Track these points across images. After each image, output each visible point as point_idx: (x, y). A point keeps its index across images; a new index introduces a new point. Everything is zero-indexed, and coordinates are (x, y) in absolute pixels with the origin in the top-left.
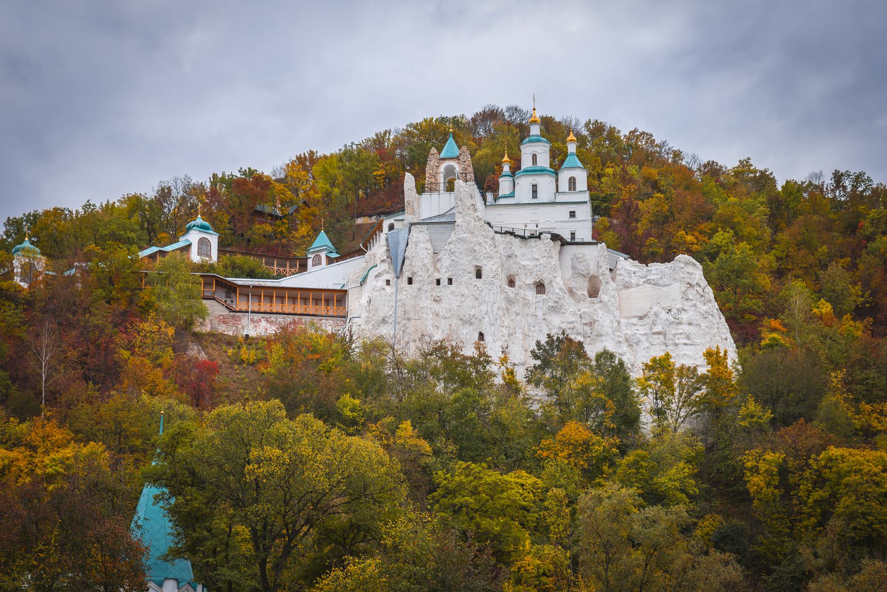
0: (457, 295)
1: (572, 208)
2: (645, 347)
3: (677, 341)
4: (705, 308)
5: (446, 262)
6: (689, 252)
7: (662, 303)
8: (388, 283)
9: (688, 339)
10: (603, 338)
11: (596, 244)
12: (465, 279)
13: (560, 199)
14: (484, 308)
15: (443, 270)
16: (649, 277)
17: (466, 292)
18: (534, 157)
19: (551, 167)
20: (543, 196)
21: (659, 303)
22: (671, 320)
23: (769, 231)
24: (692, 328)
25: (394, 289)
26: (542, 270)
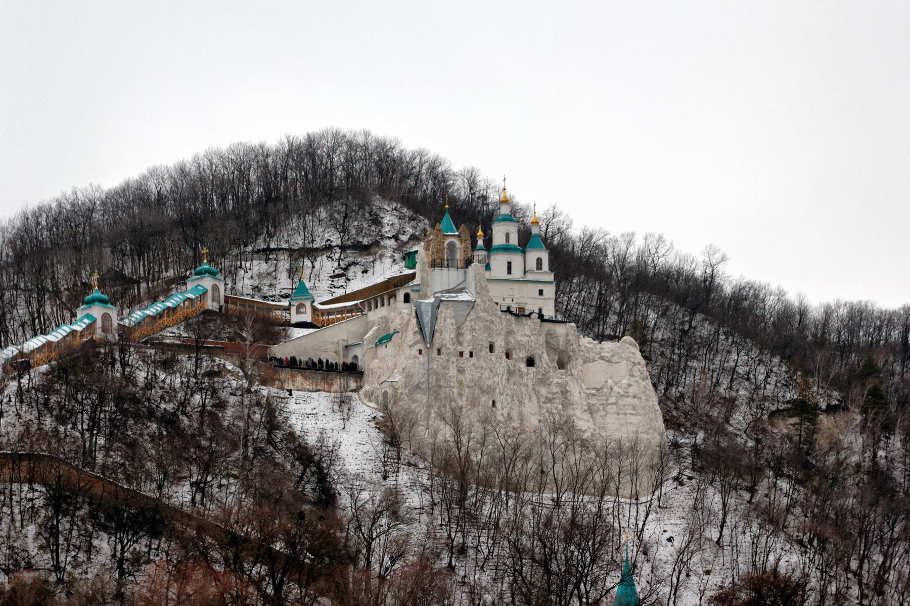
0: (477, 368)
1: (541, 287)
4: (644, 383)
5: (468, 337)
6: (643, 342)
10: (575, 406)
11: (565, 322)
12: (483, 353)
13: (529, 277)
14: (496, 379)
15: (466, 344)
16: (603, 354)
17: (484, 365)
18: (507, 235)
19: (519, 245)
20: (517, 273)
24: (636, 400)
25: (426, 358)
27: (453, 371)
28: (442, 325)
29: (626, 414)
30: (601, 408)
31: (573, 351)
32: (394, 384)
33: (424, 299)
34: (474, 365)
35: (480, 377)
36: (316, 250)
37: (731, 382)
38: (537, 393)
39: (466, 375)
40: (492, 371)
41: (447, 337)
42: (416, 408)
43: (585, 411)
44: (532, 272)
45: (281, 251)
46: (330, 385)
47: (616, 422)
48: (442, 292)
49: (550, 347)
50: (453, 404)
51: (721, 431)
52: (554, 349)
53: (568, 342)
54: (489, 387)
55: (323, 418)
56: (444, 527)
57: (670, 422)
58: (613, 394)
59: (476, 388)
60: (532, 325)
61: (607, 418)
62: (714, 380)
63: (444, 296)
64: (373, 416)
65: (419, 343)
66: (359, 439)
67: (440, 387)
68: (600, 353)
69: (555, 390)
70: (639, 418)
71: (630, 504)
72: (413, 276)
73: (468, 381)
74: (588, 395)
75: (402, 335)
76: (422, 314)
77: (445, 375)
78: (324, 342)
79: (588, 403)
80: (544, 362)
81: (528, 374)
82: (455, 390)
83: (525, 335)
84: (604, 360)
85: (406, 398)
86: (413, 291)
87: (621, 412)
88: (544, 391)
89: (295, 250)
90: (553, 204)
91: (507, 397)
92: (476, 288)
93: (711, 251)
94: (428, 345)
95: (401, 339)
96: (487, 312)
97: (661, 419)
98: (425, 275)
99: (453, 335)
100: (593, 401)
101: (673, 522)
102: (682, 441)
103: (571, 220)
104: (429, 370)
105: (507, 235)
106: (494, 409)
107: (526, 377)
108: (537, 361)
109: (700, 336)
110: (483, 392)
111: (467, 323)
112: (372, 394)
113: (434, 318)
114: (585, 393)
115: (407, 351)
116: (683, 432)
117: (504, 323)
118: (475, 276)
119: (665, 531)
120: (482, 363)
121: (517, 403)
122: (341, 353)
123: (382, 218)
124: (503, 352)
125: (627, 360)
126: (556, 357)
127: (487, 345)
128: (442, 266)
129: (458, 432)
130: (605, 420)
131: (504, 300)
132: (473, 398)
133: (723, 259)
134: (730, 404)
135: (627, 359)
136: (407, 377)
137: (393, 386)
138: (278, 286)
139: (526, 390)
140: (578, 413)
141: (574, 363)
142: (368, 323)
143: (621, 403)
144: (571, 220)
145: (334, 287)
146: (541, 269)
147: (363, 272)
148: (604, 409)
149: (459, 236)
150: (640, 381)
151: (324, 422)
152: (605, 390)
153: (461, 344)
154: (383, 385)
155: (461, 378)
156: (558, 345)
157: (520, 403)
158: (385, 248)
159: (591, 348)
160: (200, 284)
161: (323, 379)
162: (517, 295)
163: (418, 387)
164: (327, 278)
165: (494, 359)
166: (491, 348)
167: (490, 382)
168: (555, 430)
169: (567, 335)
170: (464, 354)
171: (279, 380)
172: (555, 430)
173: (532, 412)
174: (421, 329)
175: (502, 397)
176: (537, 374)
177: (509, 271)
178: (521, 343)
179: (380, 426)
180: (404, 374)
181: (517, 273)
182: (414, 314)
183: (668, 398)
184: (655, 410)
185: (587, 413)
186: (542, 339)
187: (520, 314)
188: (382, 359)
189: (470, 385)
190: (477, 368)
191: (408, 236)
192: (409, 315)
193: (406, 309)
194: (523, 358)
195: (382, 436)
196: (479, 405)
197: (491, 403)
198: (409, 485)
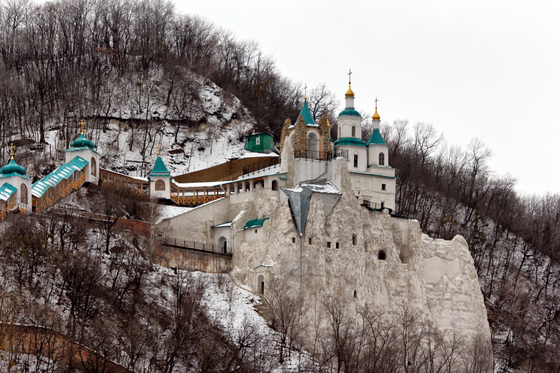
0: (343, 259)
2: (439, 309)
3: (459, 307)
4: (473, 281)
7: (449, 275)
8: (294, 239)
9: (466, 306)
10: (417, 300)
12: (348, 245)
13: (373, 171)
14: (358, 270)
15: (333, 236)
16: (438, 251)
20: (362, 167)
21: (446, 274)
22: (455, 290)
23: (338, 158)
24: (467, 297)
25: (299, 246)
26: (385, 240)
28: (313, 215)
29: (459, 310)
31: (416, 247)
32: (270, 269)
33: (290, 188)
34: (340, 256)
35: (346, 268)
38: (388, 286)
39: (334, 265)
40: (354, 262)
41: (318, 227)
44: (376, 166)
45: (111, 120)
46: (206, 265)
50: (322, 292)
53: (410, 237)
58: (448, 290)
60: (384, 219)
64: (250, 298)
65: (293, 231)
67: (311, 275)
68: (435, 250)
70: (469, 314)
73: (335, 271)
75: (272, 221)
77: (315, 264)
78: (195, 222)
80: (394, 256)
81: (380, 266)
82: (324, 279)
83: (378, 229)
86: (281, 179)
87: (455, 308)
88: (393, 283)
89: (124, 120)
90: (322, 84)
92: (342, 181)
93: (477, 145)
94: (301, 234)
95: (271, 225)
96: (351, 206)
98: (292, 164)
99: (322, 226)
100: (431, 296)
104: (301, 258)
105: (354, 128)
107: (378, 270)
108: (388, 254)
110: (348, 282)
111: (334, 215)
112: (245, 276)
113: (305, 208)
114: (425, 287)
115: (282, 239)
121: (371, 294)
122: (209, 233)
125: (459, 258)
132: (340, 287)
133: (488, 154)
135: (460, 258)
136: (282, 264)
137: (269, 272)
139: (378, 282)
141: (417, 258)
142: (230, 205)
143: (455, 299)
145: (175, 162)
146: (383, 164)
148: (440, 303)
149: (319, 128)
150: (470, 279)
152: (442, 286)
153: (328, 234)
154: (258, 270)
155: (329, 268)
156: (401, 239)
159: (428, 245)
160: (80, 156)
161: (200, 259)
162: (363, 188)
163: (291, 273)
167: (353, 273)
169: (410, 230)
170: (331, 244)
175: (361, 287)
178: (374, 236)
180: (280, 261)
181: (362, 167)
189: (337, 275)
190: (343, 259)
193: (274, 196)
194: (376, 251)
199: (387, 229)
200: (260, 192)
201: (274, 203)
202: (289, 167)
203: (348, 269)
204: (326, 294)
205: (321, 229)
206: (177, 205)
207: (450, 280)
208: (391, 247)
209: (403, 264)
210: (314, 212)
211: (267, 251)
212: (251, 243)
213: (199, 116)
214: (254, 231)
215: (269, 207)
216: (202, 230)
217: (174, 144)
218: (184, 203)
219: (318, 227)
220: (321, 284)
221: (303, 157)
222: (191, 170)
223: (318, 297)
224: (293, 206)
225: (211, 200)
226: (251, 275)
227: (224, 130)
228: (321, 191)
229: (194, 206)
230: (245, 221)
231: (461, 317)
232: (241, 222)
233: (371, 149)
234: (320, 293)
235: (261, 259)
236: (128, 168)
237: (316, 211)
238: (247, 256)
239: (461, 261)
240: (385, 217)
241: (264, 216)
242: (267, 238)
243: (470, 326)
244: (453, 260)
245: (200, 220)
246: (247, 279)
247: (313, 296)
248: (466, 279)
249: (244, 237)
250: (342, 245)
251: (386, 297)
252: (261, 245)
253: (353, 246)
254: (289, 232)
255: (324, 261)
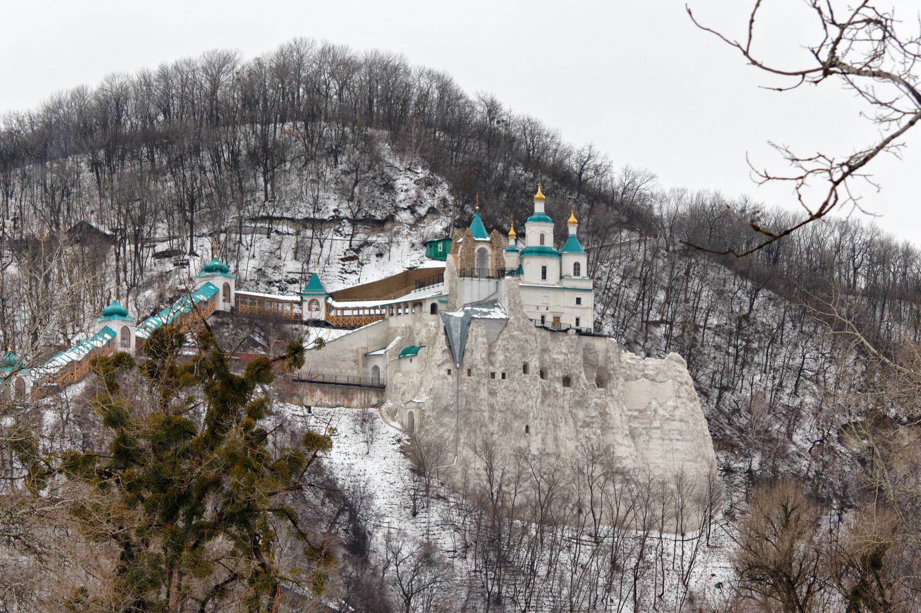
1: (578, 295)
3: (671, 436)
4: (692, 405)
5: (500, 357)
7: (659, 399)
8: (449, 372)
9: (681, 435)
10: (615, 431)
12: (516, 375)
13: (566, 284)
14: (530, 403)
15: (498, 365)
16: (646, 372)
20: (552, 278)
24: (682, 424)
25: (455, 379)
26: (570, 365)
27: (484, 394)
28: (472, 344)
29: (671, 440)
30: (644, 432)
31: (614, 369)
32: (421, 405)
34: (506, 387)
36: (322, 221)
37: (796, 386)
38: (574, 417)
40: (525, 394)
41: (478, 357)
42: (444, 432)
43: (627, 435)
44: (570, 279)
46: (350, 400)
47: (660, 448)
48: (473, 304)
49: (588, 363)
50: (484, 429)
51: (781, 453)
52: (592, 365)
53: (607, 359)
54: (522, 411)
55: (345, 440)
56: (477, 573)
57: (721, 443)
58: (657, 417)
59: (509, 413)
60: (570, 341)
61: (651, 443)
62: (777, 381)
63: (477, 312)
64: (397, 438)
66: (385, 466)
67: (470, 410)
68: (643, 370)
69: (594, 414)
70: (685, 444)
71: (676, 541)
72: (436, 276)
73: (500, 404)
74: (630, 417)
75: (428, 349)
76: (450, 329)
77: (475, 398)
78: (343, 351)
79: (630, 427)
80: (581, 382)
81: (564, 395)
82: (486, 414)
83: (562, 353)
84: (647, 378)
85: (434, 422)
87: (666, 437)
88: (581, 414)
90: (589, 143)
91: (542, 421)
92: (509, 304)
96: (521, 331)
97: (710, 444)
98: (454, 285)
99: (484, 355)
100: (635, 424)
101: (722, 564)
102: (736, 465)
103: (611, 163)
104: (458, 391)
106: (527, 435)
107: (561, 399)
109: (762, 323)
110: (516, 417)
111: (499, 342)
113: (464, 336)
114: (626, 415)
115: (436, 372)
116: (736, 455)
117: (539, 340)
118: (509, 292)
119: (713, 575)
120: (515, 385)
121: (552, 427)
122: (361, 362)
123: (395, 180)
124: (537, 373)
125: (673, 379)
126: (595, 374)
127: (521, 366)
128: (472, 275)
129: (490, 468)
130: (648, 445)
131: (538, 308)
134: (794, 416)
136: (434, 399)
137: (419, 408)
138: (285, 269)
139: (562, 413)
140: (619, 438)
141: (615, 382)
142: (389, 328)
143: (666, 427)
144: (611, 163)
146: (579, 275)
147: (378, 255)
148: (647, 433)
151: (347, 445)
152: (649, 413)
153: (492, 364)
154: (408, 405)
155: (492, 400)
156: (597, 361)
157: (555, 426)
158: (400, 223)
159: (634, 365)
161: (343, 393)
162: (552, 304)
163: (446, 409)
164: (337, 261)
165: (527, 380)
166: (525, 369)
167: (523, 407)
168: (593, 460)
169: (607, 351)
170: (496, 375)
171: (298, 395)
172: (593, 460)
173: (569, 436)
174: (450, 347)
175: (536, 421)
176: (574, 396)
177: (544, 276)
178: (557, 361)
179: (404, 451)
181: (552, 278)
182: (442, 331)
183: (721, 412)
184: (704, 434)
185: (629, 437)
186: (579, 358)
187: (556, 329)
188: (406, 374)
190: (510, 391)
191: (426, 208)
192: (437, 328)
194: (559, 378)
195: (408, 462)
196: (511, 430)
197: (524, 428)
198: (439, 523)
199: (572, 352)
200: (419, 315)
201: (432, 328)
202: (451, 289)
203: (517, 401)
204: (489, 431)
205: (483, 359)
206: (334, 328)
207: (661, 405)
208: (578, 373)
209: (600, 389)
210: (474, 340)
211: (421, 383)
212: (406, 374)
213: (386, 214)
214: (408, 360)
215: (426, 333)
216: (352, 358)
217: (347, 250)
218: (341, 325)
219: (478, 357)
220: (482, 420)
221: (470, 276)
222: (364, 282)
223: (478, 435)
224: (451, 333)
225: (370, 322)
226: (402, 410)
227: (414, 229)
228: (488, 317)
229: (353, 328)
230: (400, 349)
231: (675, 447)
232: (396, 350)
233: (564, 258)
234: (481, 430)
235: (413, 392)
236: (288, 282)
237: (476, 339)
238: (400, 388)
239: (675, 383)
240: (570, 339)
241: (420, 343)
242: (423, 369)
243: (687, 458)
244: (665, 381)
245: (349, 348)
246: (397, 415)
247: (471, 434)
248: (682, 403)
249: (399, 366)
250: (509, 375)
251: (572, 428)
252: (415, 377)
253: (523, 375)
254: (443, 364)
255: (486, 395)
